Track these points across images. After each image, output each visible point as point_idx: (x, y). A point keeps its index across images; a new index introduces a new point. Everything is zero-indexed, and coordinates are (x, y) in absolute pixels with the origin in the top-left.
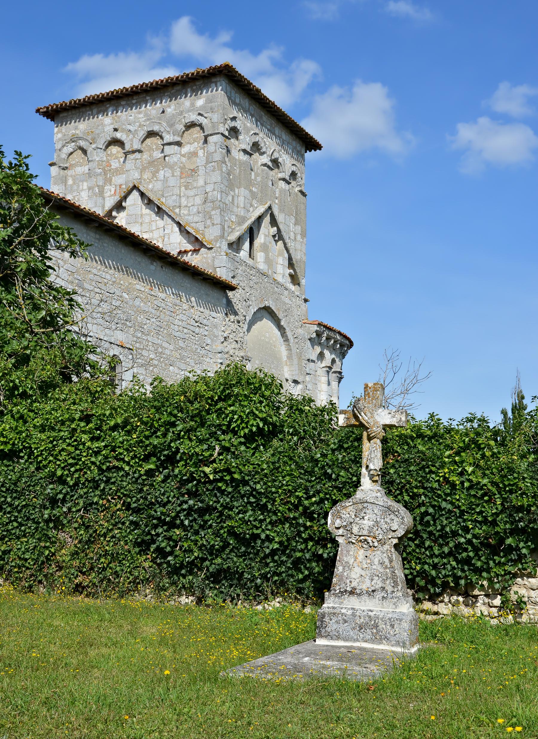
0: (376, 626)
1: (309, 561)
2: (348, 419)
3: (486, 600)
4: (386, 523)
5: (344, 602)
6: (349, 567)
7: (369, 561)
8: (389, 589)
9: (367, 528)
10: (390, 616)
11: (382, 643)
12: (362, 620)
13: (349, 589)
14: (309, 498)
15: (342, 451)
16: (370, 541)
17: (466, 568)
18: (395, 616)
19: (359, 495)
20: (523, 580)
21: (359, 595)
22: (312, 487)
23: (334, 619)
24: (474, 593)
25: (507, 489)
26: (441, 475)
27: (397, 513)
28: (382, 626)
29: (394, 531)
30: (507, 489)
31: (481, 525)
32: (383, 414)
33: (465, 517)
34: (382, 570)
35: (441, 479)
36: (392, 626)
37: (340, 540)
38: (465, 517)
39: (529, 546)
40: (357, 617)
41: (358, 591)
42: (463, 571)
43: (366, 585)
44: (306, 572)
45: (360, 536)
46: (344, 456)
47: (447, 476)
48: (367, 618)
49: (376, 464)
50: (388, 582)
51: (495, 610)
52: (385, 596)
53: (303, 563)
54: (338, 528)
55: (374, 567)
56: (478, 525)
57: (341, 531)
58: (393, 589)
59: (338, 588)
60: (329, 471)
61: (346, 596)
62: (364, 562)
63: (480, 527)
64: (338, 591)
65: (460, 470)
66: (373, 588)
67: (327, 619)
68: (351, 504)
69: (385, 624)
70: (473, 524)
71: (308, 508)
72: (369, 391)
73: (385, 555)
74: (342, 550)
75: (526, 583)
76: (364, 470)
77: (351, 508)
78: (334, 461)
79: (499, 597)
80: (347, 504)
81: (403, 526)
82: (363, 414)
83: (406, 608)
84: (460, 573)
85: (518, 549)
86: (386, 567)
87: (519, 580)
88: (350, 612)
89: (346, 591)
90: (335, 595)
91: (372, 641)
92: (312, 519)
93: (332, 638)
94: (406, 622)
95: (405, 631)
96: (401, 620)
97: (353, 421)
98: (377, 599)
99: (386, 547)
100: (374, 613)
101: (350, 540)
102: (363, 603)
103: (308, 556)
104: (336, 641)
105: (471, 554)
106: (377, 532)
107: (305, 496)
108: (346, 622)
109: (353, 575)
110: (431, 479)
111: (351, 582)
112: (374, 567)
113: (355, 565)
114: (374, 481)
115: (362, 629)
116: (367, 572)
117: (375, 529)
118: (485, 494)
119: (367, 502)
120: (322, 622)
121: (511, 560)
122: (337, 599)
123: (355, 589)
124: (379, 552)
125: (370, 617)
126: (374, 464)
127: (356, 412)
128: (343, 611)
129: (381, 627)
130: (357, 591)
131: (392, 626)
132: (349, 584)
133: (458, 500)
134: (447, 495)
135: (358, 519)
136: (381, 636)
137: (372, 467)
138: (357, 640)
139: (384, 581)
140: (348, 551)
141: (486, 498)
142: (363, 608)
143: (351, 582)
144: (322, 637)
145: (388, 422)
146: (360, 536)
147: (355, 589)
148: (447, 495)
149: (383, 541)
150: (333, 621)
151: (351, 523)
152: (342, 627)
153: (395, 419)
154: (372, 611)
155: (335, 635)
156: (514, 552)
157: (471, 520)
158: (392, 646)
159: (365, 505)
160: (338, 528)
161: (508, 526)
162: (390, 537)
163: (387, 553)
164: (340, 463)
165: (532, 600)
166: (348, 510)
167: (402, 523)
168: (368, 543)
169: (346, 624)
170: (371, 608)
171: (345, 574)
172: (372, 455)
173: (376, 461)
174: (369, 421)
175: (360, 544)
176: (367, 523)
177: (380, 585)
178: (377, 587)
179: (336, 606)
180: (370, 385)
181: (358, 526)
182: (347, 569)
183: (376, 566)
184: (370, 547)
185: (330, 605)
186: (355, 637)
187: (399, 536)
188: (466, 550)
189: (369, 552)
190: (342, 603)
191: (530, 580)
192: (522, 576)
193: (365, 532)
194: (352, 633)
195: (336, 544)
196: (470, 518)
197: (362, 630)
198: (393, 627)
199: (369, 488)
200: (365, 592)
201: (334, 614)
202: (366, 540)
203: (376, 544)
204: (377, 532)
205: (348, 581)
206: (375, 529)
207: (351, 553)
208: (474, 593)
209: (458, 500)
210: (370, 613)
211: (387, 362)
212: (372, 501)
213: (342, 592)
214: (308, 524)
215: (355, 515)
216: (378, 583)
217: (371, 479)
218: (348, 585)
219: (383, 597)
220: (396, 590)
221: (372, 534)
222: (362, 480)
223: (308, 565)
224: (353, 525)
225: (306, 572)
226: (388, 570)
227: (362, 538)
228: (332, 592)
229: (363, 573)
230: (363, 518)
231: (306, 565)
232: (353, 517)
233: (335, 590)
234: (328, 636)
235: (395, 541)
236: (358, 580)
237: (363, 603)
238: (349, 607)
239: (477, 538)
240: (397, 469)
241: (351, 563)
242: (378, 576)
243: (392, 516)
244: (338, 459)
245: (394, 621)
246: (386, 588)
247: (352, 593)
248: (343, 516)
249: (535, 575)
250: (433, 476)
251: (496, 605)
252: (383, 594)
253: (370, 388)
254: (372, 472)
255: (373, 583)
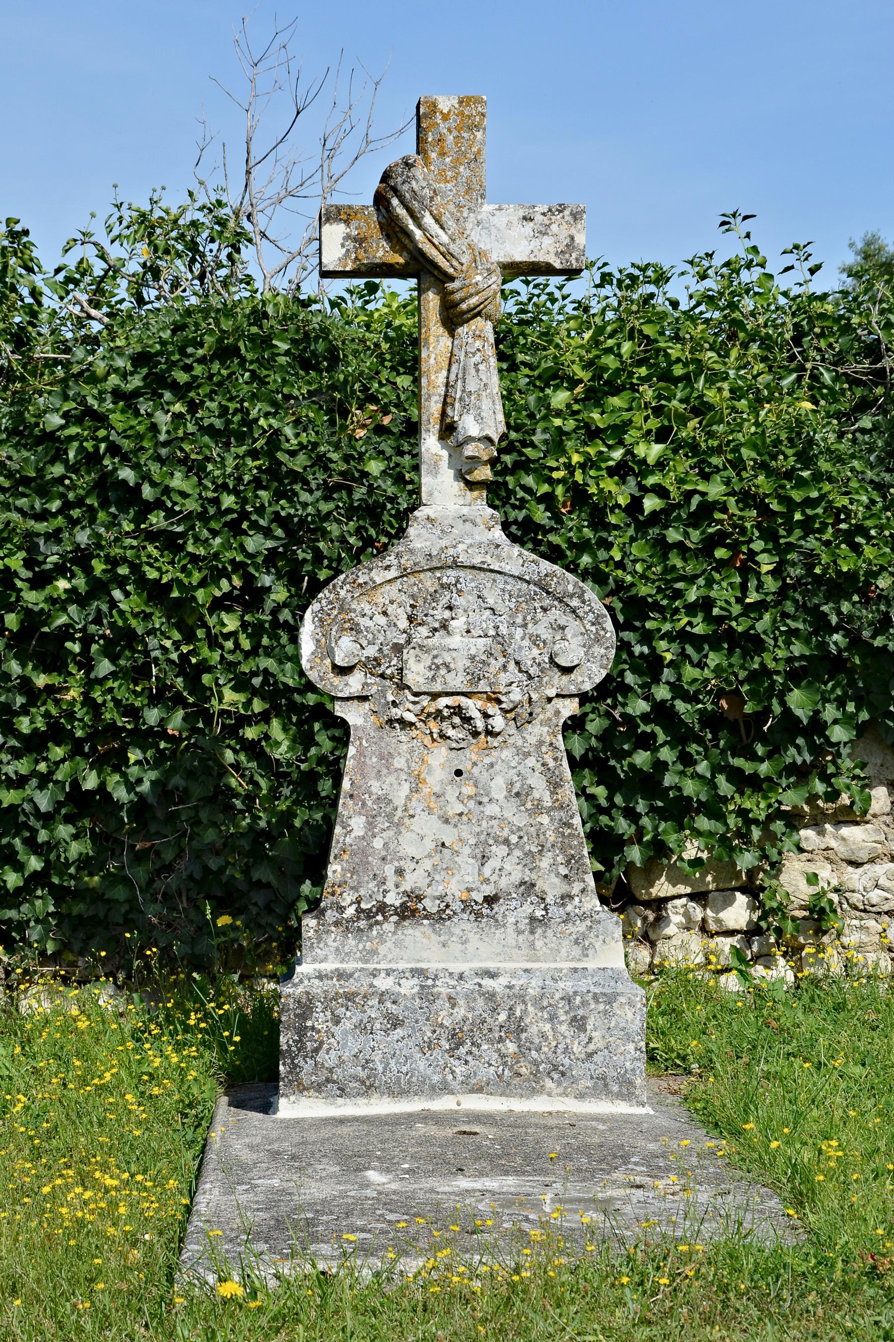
0: (517, 1029)
1: (47, 819)
2: (360, 240)
3: (698, 913)
4: (535, 640)
5: (382, 950)
6: (390, 816)
7: (469, 790)
8: (552, 887)
9: (462, 663)
10: (566, 986)
11: (541, 1090)
12: (461, 1012)
13: (393, 899)
14: (40, 581)
15: (168, 396)
16: (476, 714)
17: (641, 806)
18: (584, 985)
19: (419, 537)
20: (822, 833)
21: (440, 917)
22: (54, 536)
23: (351, 1018)
24: (654, 891)
25: (798, 516)
26: (556, 475)
27: (575, 603)
28: (537, 1025)
29: (567, 670)
30: (798, 516)
31: (699, 649)
32: (500, 220)
33: (649, 625)
34: (521, 820)
35: (560, 490)
36: (579, 1024)
37: (353, 715)
38: (649, 625)
39: (852, 717)
40: (442, 1003)
41: (431, 906)
42: (632, 815)
43: (462, 880)
44: (35, 864)
45: (435, 696)
46: (178, 416)
47: (579, 477)
48: (481, 1002)
49: (483, 421)
50: (545, 863)
51: (726, 944)
52: (539, 913)
53: (18, 828)
54: (343, 671)
55: (491, 809)
56: (689, 650)
57: (355, 683)
58: (564, 888)
59: (348, 898)
60: (127, 474)
61: (388, 927)
62: (451, 794)
63: (695, 657)
64: (351, 911)
65: (618, 454)
66: (489, 890)
67: (320, 1020)
68: (393, 573)
69: (552, 1018)
70: (675, 646)
71: (42, 617)
72: (443, 128)
73: (531, 761)
74: (361, 753)
75: (833, 844)
76: (431, 443)
77: (392, 591)
78: (140, 437)
79: (741, 899)
80: (379, 576)
81: (598, 650)
82: (428, 220)
83: (610, 950)
84: (623, 826)
85: (817, 725)
86: (538, 808)
87: (808, 835)
88: (409, 987)
89: (382, 908)
90: (345, 926)
91: (501, 1086)
92: (54, 662)
93: (343, 1092)
94: (631, 1004)
95: (629, 1038)
96: (610, 999)
97: (382, 251)
98: (510, 929)
99: (536, 731)
100: (503, 981)
101: (396, 713)
102: (455, 947)
103: (44, 802)
104: (361, 1101)
105: (666, 754)
106: (504, 678)
107: (25, 574)
108: (396, 1022)
109: (409, 846)
110: (521, 494)
111: (400, 872)
112: (491, 809)
113: (416, 806)
114: (471, 485)
115: (461, 1043)
116: (465, 831)
117: (495, 665)
118: (719, 540)
119: (456, 565)
120: (302, 1031)
121: (792, 769)
122: (351, 941)
123: (419, 898)
124: (506, 754)
125: (491, 996)
126: (479, 419)
127: (401, 212)
128: (383, 983)
129: (534, 1030)
130: (427, 903)
131: (579, 1024)
132: (391, 880)
133: (620, 565)
134: (583, 546)
135: (424, 631)
136: (536, 1064)
137: (470, 426)
138: (444, 1088)
139: (529, 859)
140: (386, 758)
141: (721, 553)
142: (457, 967)
143: (400, 872)
144: (302, 1089)
145: (521, 254)
146: (435, 696)
147: (419, 898)
148: (583, 546)
149: (524, 712)
150: (347, 1025)
151: (398, 649)
152: (384, 1046)
153: (547, 241)
154: (493, 975)
155: (355, 1078)
156: (800, 741)
157: (668, 637)
158: (581, 1096)
159: (450, 576)
160: (343, 671)
161: (798, 649)
162: (552, 693)
163: (540, 755)
164: (166, 444)
165: (855, 898)
166: (380, 598)
167: (598, 640)
168: (467, 720)
169: (399, 1032)
170: (491, 965)
171: (378, 843)
172: (466, 387)
173: (486, 404)
174: (454, 248)
175: (434, 726)
176: (461, 645)
177: (516, 877)
178: (504, 883)
179: (349, 966)
180: (445, 104)
181: (427, 660)
182: (382, 823)
183: (501, 808)
184: (475, 734)
185: (328, 967)
186: (436, 1078)
187: (587, 687)
188: (646, 742)
189: (471, 754)
190: (374, 952)
191: (845, 831)
192: (817, 822)
193: (457, 682)
194: (422, 1065)
195: (342, 732)
196: (667, 627)
197: (462, 1050)
198: (582, 1028)
199: (449, 508)
200: (457, 906)
201: (350, 997)
202: (458, 710)
203: (498, 722)
204: (504, 678)
205: (389, 871)
206: (495, 665)
207: (399, 762)
208: (654, 891)
209: (620, 565)
210: (487, 983)
211: (250, 72)
212: (477, 561)
213: (369, 914)
214: (41, 680)
215: (411, 619)
216: (507, 870)
217: (460, 476)
218: (390, 884)
219: (532, 919)
220: (576, 888)
221: (483, 686)
222: (427, 481)
223: (43, 836)
224: (409, 655)
225: (35, 864)
226: (545, 819)
227: (443, 702)
228: (331, 916)
229: (449, 835)
230: (444, 626)
231: (34, 832)
232: (403, 624)
233: (341, 909)
234: (330, 1085)
235: (570, 708)
236: (427, 864)
237: (455, 947)
238: (401, 966)
239: (692, 699)
240: (389, 459)
241: (399, 801)
242: (506, 842)
243: (557, 614)
244: (154, 428)
245: (584, 1003)
246: (540, 885)
247: (408, 911)
248: (364, 622)
249: (865, 812)
250: (529, 480)
251: (732, 925)
252: (527, 909)
253: (445, 117)
254: (470, 450)
255: (487, 871)
